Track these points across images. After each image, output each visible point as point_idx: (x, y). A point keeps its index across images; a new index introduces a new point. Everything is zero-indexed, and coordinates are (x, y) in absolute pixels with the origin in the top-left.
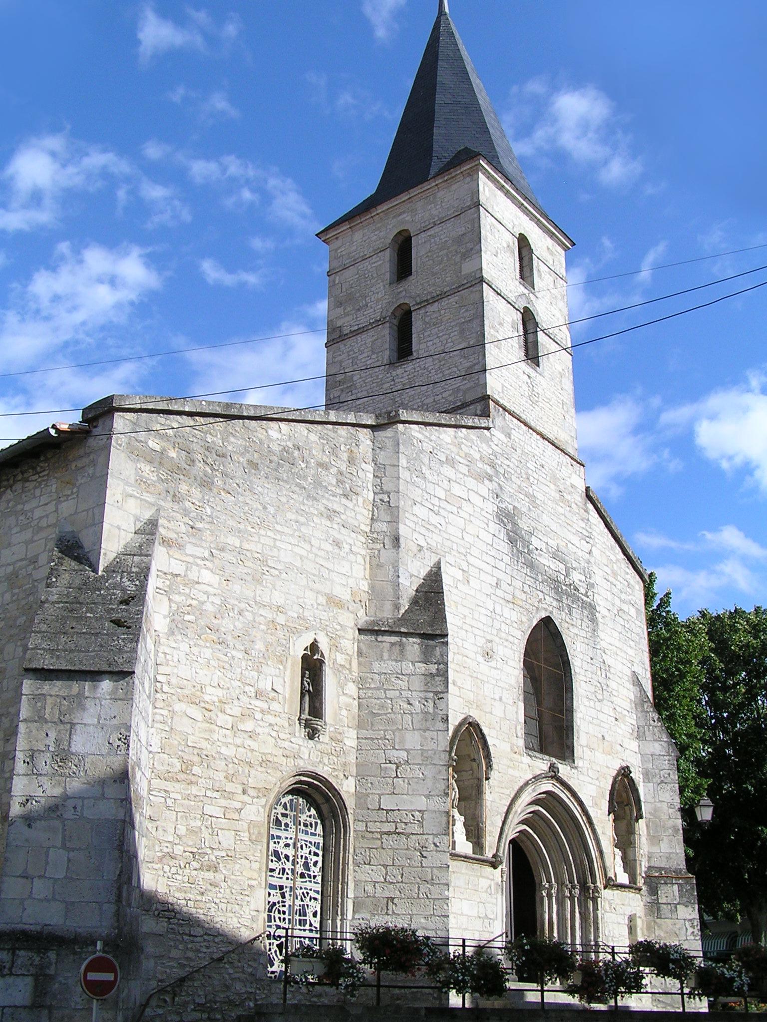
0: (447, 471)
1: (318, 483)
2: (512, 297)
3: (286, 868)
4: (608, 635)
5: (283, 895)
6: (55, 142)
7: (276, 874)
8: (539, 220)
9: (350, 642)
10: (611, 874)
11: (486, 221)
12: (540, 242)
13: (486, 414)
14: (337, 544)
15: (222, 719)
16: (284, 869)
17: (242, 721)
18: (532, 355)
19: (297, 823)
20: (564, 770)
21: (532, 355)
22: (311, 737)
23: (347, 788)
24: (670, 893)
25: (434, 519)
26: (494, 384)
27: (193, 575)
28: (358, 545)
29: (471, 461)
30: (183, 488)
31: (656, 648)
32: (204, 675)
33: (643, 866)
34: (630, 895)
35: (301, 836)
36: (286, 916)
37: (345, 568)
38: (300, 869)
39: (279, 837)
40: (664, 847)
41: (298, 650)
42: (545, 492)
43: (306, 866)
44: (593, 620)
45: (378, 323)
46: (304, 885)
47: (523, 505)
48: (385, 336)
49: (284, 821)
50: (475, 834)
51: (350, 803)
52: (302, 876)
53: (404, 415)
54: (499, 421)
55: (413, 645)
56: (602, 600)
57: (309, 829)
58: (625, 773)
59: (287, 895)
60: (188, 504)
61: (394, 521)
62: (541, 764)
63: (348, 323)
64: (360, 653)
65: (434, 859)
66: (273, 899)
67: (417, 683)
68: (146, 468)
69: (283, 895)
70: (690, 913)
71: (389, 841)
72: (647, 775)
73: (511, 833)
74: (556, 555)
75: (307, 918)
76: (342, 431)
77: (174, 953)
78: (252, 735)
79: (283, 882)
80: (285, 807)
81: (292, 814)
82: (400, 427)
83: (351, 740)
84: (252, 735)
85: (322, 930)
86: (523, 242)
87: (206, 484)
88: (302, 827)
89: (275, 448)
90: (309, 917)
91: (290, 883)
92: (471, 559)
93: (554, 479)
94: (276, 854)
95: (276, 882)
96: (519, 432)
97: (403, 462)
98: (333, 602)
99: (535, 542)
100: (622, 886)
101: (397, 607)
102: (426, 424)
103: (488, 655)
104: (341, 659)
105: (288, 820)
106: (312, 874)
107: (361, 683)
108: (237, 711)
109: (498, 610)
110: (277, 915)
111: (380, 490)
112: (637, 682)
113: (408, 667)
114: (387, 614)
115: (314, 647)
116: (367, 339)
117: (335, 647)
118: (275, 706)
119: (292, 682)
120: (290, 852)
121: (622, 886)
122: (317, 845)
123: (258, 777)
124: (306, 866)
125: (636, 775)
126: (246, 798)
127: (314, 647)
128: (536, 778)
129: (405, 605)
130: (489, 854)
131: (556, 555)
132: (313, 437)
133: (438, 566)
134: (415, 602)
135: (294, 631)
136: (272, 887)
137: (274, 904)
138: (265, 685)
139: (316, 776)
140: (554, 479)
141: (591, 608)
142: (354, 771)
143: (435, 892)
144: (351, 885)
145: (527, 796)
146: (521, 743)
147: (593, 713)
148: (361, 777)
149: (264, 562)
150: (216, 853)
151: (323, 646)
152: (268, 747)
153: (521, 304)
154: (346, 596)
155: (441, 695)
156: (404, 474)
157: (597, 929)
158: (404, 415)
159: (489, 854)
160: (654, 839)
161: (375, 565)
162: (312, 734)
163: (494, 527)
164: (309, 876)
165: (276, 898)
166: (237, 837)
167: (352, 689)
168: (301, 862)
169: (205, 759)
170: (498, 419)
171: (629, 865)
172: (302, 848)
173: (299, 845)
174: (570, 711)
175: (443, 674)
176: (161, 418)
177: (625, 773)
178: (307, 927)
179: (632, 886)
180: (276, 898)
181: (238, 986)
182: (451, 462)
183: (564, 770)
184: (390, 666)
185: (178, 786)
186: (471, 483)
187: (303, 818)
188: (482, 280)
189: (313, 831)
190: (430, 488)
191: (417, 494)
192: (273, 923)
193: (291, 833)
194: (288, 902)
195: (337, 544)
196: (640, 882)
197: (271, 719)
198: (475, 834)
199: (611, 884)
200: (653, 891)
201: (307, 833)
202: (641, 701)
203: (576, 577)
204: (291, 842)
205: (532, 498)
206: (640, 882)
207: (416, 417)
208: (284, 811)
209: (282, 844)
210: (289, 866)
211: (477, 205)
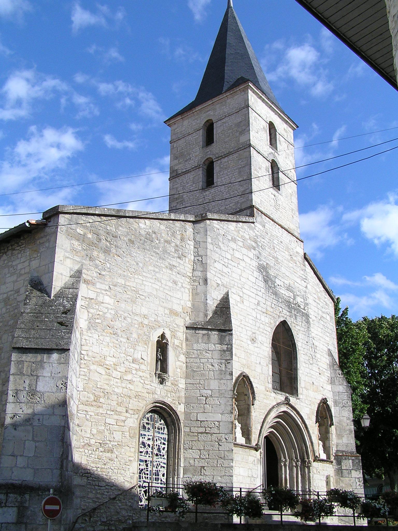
0: (232, 245)
1: (165, 251)
2: (266, 155)
3: (149, 451)
4: (316, 330)
5: (147, 465)
6: (28, 74)
7: (143, 454)
8: (280, 114)
9: (181, 333)
10: (317, 454)
11: (252, 115)
12: (280, 126)
13: (252, 215)
14: (175, 283)
15: (115, 374)
16: (147, 452)
17: (126, 375)
18: (276, 184)
19: (154, 427)
20: (293, 400)
21: (276, 184)
22: (161, 383)
23: (180, 409)
24: (348, 464)
25: (225, 270)
26: (256, 199)
27: (100, 299)
28: (186, 283)
29: (244, 239)
30: (95, 253)
31: (340, 337)
32: (106, 351)
33: (333, 450)
34: (327, 465)
35: (156, 434)
36: (149, 476)
37: (179, 295)
38: (156, 452)
39: (145, 435)
40: (345, 440)
41: (155, 338)
42: (283, 256)
43: (159, 450)
44: (308, 322)
45: (196, 168)
46: (158, 460)
47: (271, 262)
48: (200, 175)
49: (147, 426)
50: (246, 433)
51: (182, 417)
52: (157, 455)
53: (210, 216)
54: (259, 219)
55: (214, 335)
56: (312, 312)
57: (160, 431)
58: (324, 402)
59: (149, 465)
60: (97, 262)
61: (205, 271)
62: (281, 397)
63: (180, 168)
64: (187, 339)
65: (225, 446)
66: (142, 467)
67: (217, 355)
68: (76, 243)
69: (147, 465)
70: (358, 474)
71: (202, 437)
72: (336, 403)
73: (265, 433)
74: (289, 288)
75: (159, 477)
76: (178, 224)
77: (91, 495)
78: (131, 382)
79: (147, 458)
80: (148, 419)
81: (152, 423)
82: (208, 222)
83: (182, 384)
84: (131, 382)
85: (167, 483)
86: (271, 126)
87: (107, 251)
88: (157, 430)
89: (143, 233)
90: (161, 476)
91: (150, 459)
92: (245, 291)
93: (288, 249)
94: (143, 444)
95: (143, 458)
96: (269, 224)
97: (209, 240)
98: (173, 313)
99: (278, 282)
100: (323, 461)
101: (206, 315)
102: (221, 220)
103: (253, 340)
104: (177, 342)
105: (149, 426)
106: (162, 454)
107: (188, 355)
108: (123, 370)
109: (258, 317)
110: (144, 476)
111: (197, 254)
112: (330, 354)
113: (212, 347)
114: (201, 319)
115: (163, 336)
116: (190, 176)
117: (174, 336)
118: (143, 367)
119: (152, 354)
120: (151, 443)
121: (323, 461)
122: (164, 439)
123: (134, 404)
124: (159, 450)
125: (330, 403)
126: (127, 415)
127: (163, 336)
128: (278, 404)
129: (210, 315)
130: (254, 443)
131: (289, 288)
132: (162, 227)
133: (227, 294)
134: (215, 313)
135: (153, 328)
136: (141, 461)
137: (142, 470)
138: (138, 356)
139: (164, 403)
140: (288, 249)
141: (307, 316)
142: (184, 400)
143: (226, 463)
144: (182, 460)
145: (274, 414)
146: (270, 386)
147: (308, 370)
148: (187, 404)
149: (137, 292)
150: (112, 443)
151: (168, 335)
152: (139, 388)
153: (270, 158)
154: (179, 309)
155: (229, 361)
156: (210, 246)
157: (310, 483)
158: (210, 216)
159: (254, 443)
160: (339, 436)
161: (195, 293)
162: (162, 381)
163: (256, 274)
164: (161, 455)
165: (143, 467)
166: (123, 435)
167: (183, 358)
168: (156, 448)
169: (107, 394)
170: (258, 218)
171: (326, 449)
172: (157, 441)
173: (155, 439)
174: (296, 369)
175: (230, 350)
176: (84, 217)
177: (324, 402)
178: (159, 482)
179: (328, 460)
180: (143, 467)
181: (124, 512)
182: (234, 240)
183: (293, 400)
184: (202, 346)
185: (92, 408)
186: (244, 251)
187: (157, 425)
188: (250, 145)
189: (162, 432)
190: (223, 254)
191: (216, 257)
192: (142, 480)
193: (151, 433)
194: (150, 469)
195: (175, 283)
196: (332, 458)
197: (140, 374)
198: (246, 433)
199: (317, 459)
200: (339, 463)
201: (159, 433)
202: (333, 364)
203: (299, 300)
204: (151, 437)
205: (276, 259)
206: (332, 458)
207: (216, 217)
208: (147, 422)
209: (146, 439)
210: (150, 450)
211: (248, 106)
